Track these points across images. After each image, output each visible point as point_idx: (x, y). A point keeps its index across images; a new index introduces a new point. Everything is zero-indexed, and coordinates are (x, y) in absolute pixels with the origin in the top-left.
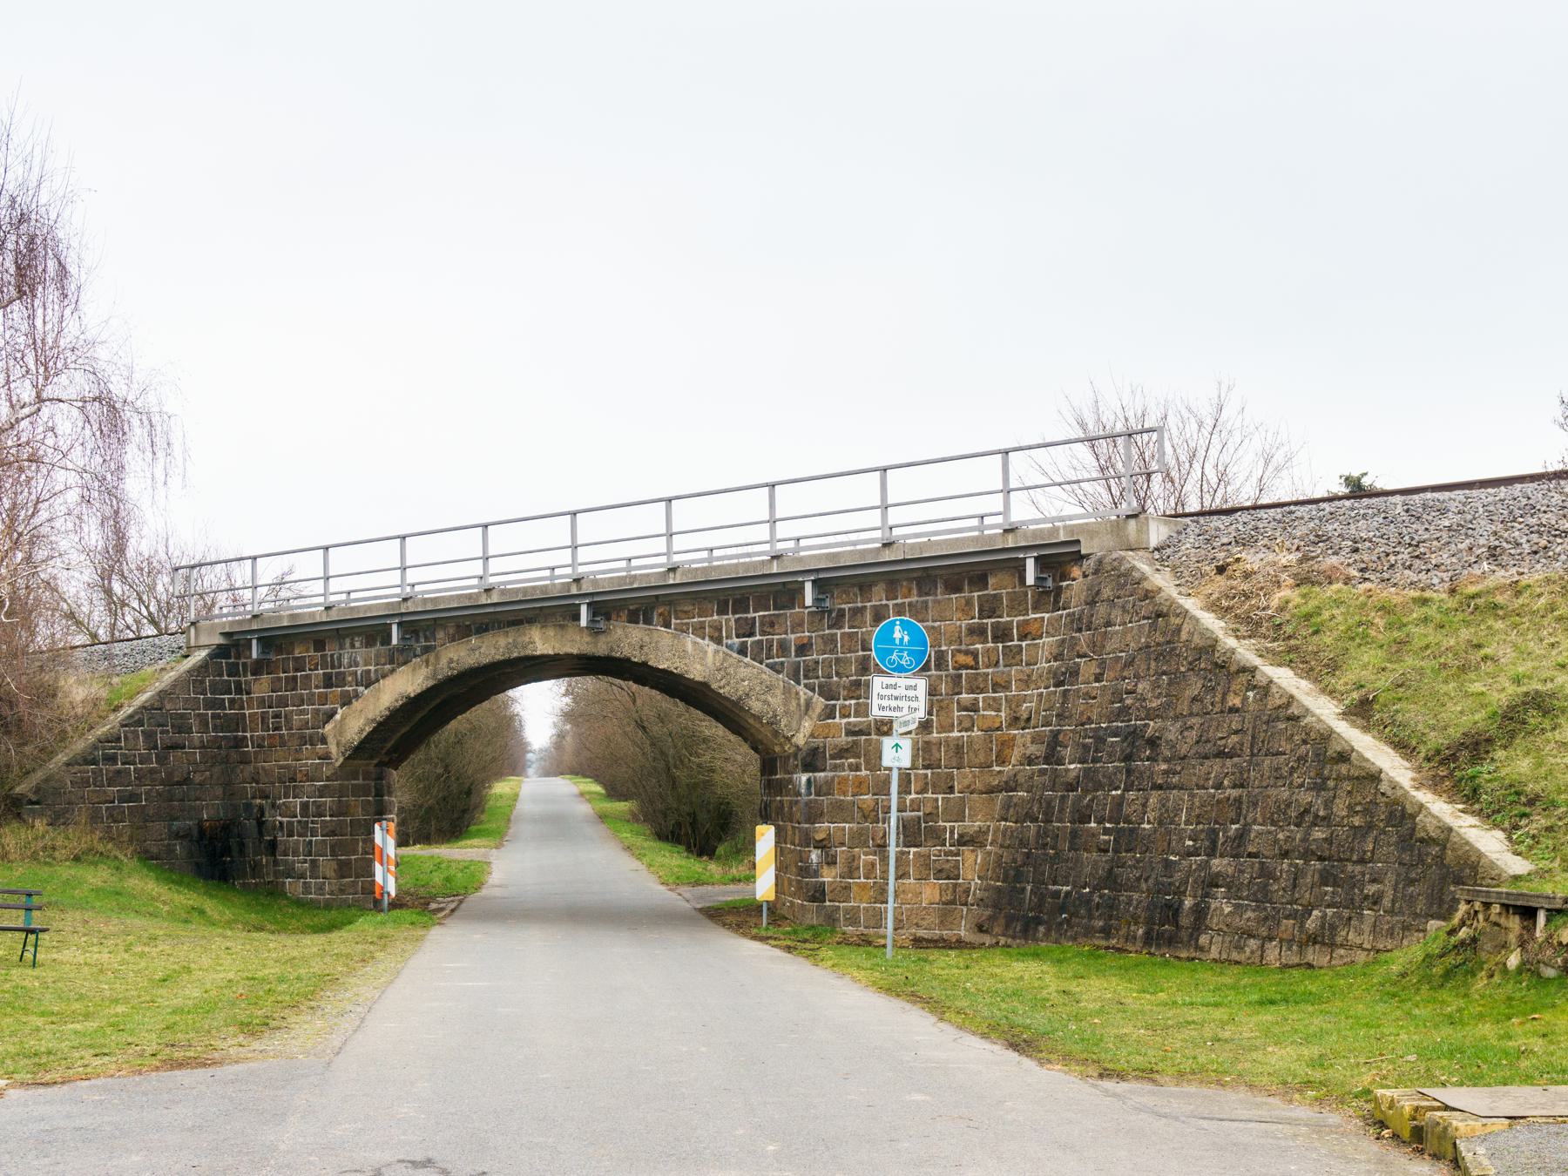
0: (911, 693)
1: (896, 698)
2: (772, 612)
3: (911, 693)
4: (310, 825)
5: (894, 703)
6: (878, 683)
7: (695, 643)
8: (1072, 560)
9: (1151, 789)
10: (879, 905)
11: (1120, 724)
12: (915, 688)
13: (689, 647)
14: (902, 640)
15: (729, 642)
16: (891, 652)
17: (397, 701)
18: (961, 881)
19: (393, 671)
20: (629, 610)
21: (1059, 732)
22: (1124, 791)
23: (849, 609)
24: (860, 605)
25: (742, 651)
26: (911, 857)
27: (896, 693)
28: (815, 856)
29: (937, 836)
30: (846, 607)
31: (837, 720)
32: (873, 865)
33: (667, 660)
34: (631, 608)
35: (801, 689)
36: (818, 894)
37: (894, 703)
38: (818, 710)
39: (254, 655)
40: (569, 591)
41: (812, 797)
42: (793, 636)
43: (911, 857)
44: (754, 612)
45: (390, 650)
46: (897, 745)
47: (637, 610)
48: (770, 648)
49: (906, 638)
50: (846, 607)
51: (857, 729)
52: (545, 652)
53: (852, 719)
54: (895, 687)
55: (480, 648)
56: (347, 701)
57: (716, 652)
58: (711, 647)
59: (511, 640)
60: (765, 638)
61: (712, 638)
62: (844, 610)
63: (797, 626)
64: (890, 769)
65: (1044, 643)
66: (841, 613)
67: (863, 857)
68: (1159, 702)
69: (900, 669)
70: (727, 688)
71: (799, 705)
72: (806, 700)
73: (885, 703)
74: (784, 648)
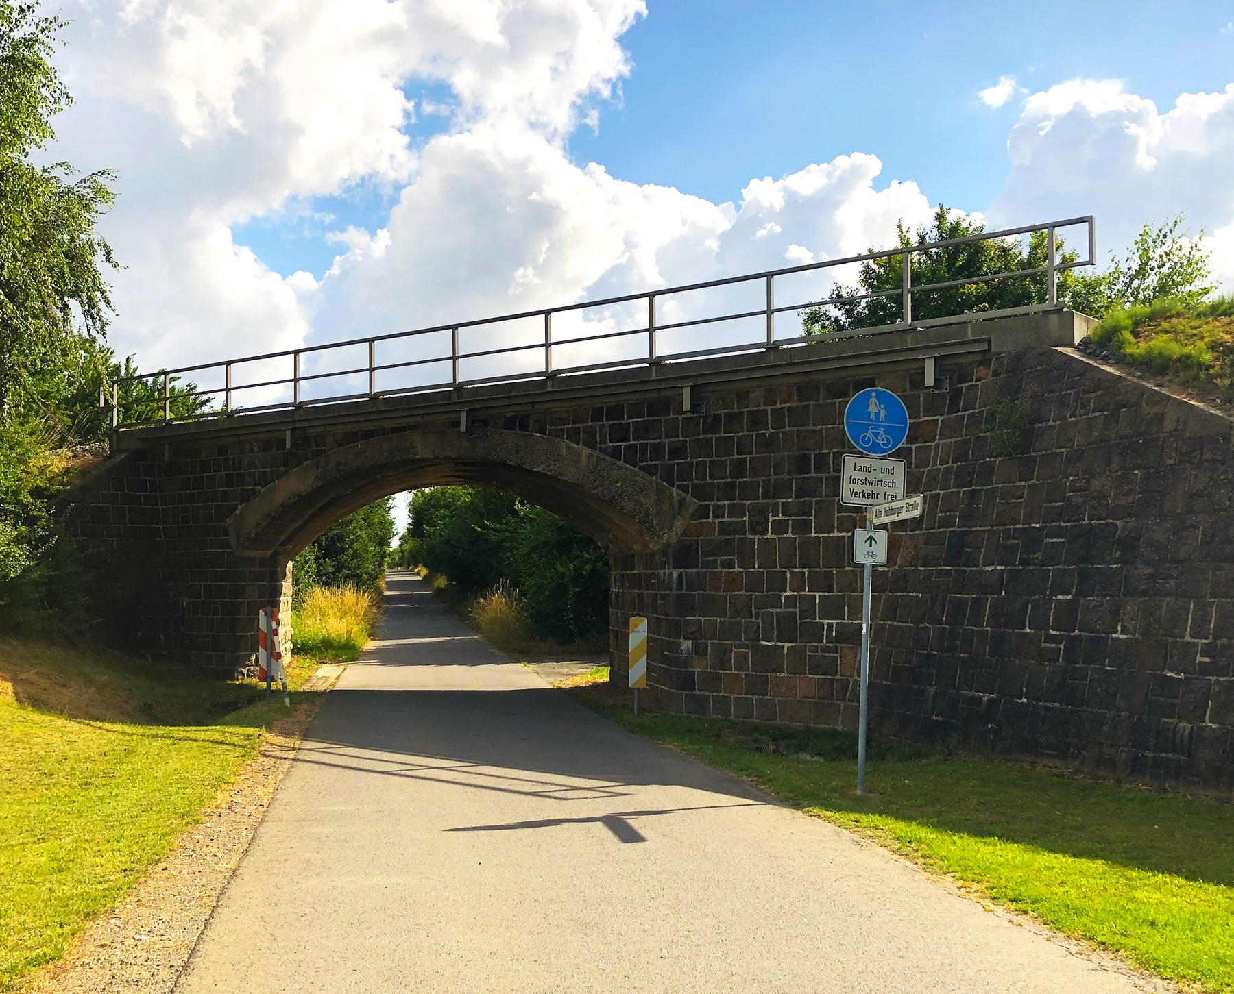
0: (888, 478)
1: (871, 483)
2: (646, 419)
3: (888, 478)
4: (213, 605)
5: (867, 489)
6: (851, 464)
7: (568, 447)
8: (37, 664)
9: (1125, 596)
10: (750, 697)
11: (1063, 524)
12: (891, 471)
13: (564, 451)
14: (877, 414)
15: (603, 446)
16: (866, 428)
17: (290, 499)
18: (838, 677)
19: (286, 473)
20: (505, 418)
21: (965, 534)
22: (1077, 595)
23: (725, 415)
24: (736, 410)
25: (616, 454)
26: (786, 651)
27: (870, 477)
28: (686, 645)
29: (815, 633)
30: (722, 412)
31: (710, 520)
32: (745, 657)
33: (542, 463)
34: (507, 415)
35: (675, 491)
36: (688, 682)
37: (867, 489)
38: (691, 510)
39: (166, 458)
40: (450, 399)
41: (684, 592)
42: (667, 441)
43: (786, 651)
44: (628, 419)
45: (284, 453)
46: (871, 538)
47: (513, 418)
48: (643, 452)
49: (883, 414)
50: (722, 412)
51: (731, 528)
52: (426, 456)
53: (726, 519)
54: (869, 469)
55: (365, 452)
56: (246, 497)
57: (590, 456)
58: (585, 451)
59: (394, 445)
60: (638, 442)
61: (586, 444)
62: (720, 415)
63: (672, 431)
64: (863, 565)
65: (937, 445)
66: (717, 418)
67: (734, 650)
68: (1130, 499)
69: (875, 448)
70: (600, 489)
71: (671, 505)
72: (679, 501)
73: (858, 488)
74: (657, 451)
